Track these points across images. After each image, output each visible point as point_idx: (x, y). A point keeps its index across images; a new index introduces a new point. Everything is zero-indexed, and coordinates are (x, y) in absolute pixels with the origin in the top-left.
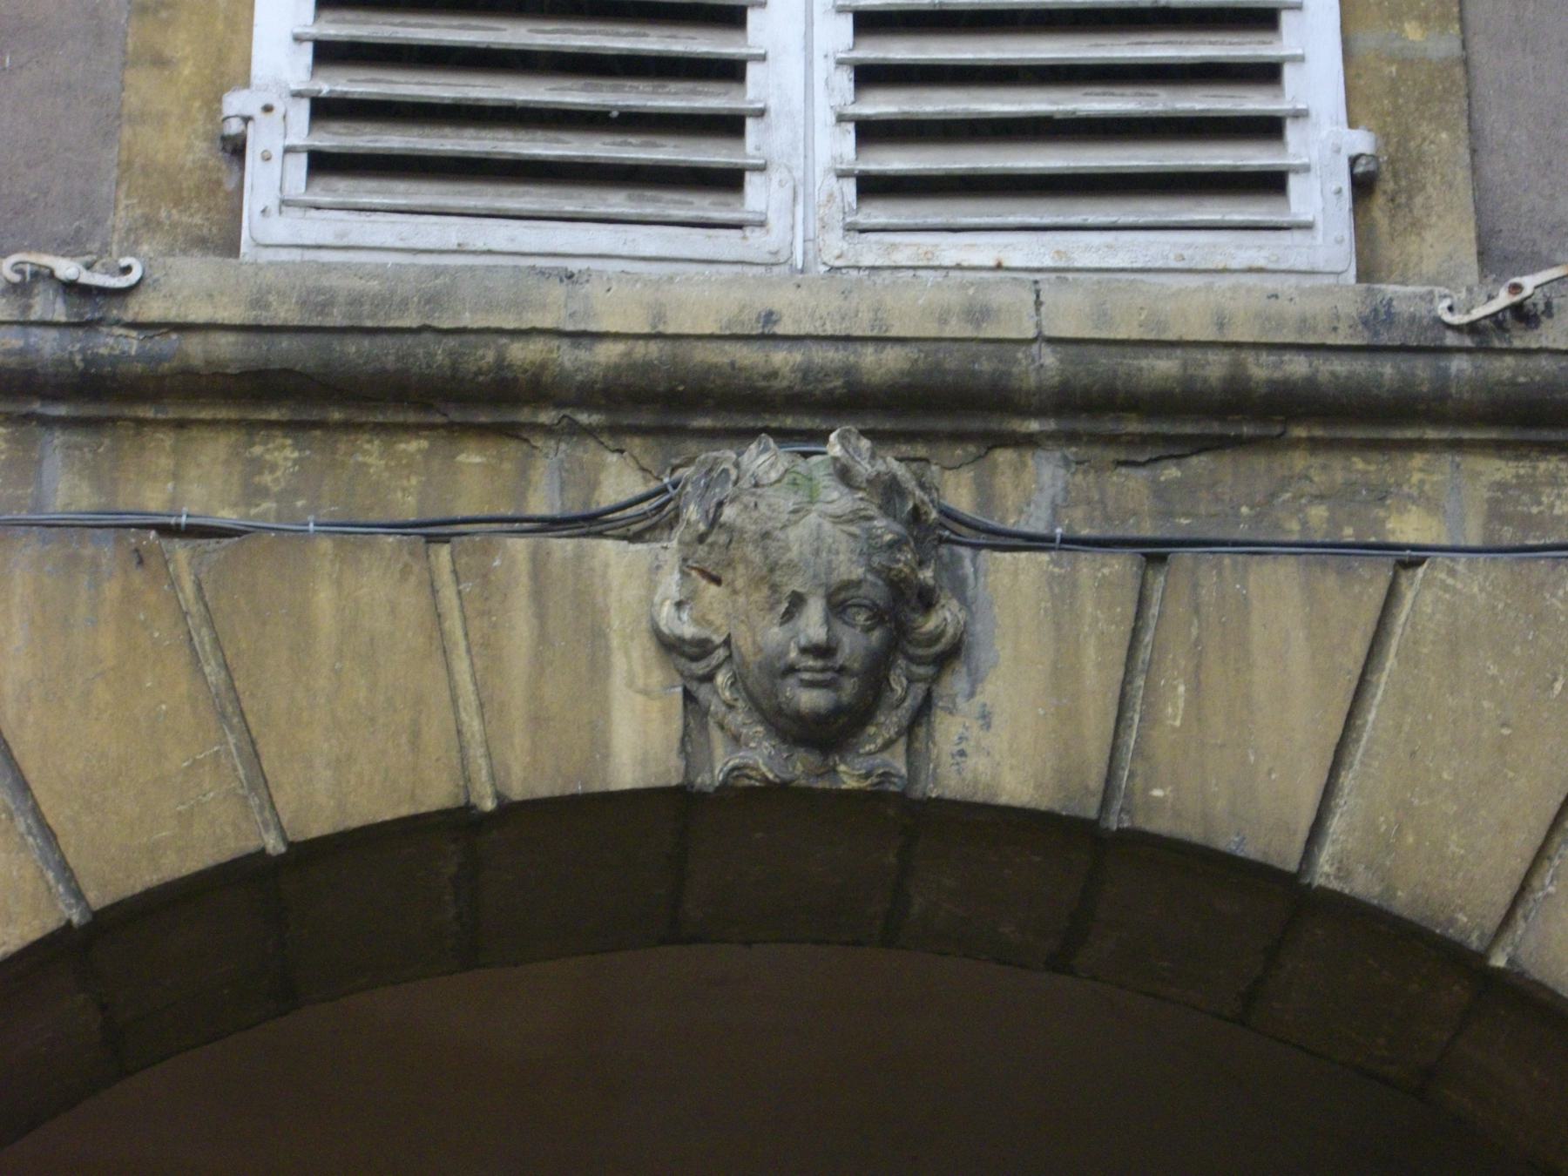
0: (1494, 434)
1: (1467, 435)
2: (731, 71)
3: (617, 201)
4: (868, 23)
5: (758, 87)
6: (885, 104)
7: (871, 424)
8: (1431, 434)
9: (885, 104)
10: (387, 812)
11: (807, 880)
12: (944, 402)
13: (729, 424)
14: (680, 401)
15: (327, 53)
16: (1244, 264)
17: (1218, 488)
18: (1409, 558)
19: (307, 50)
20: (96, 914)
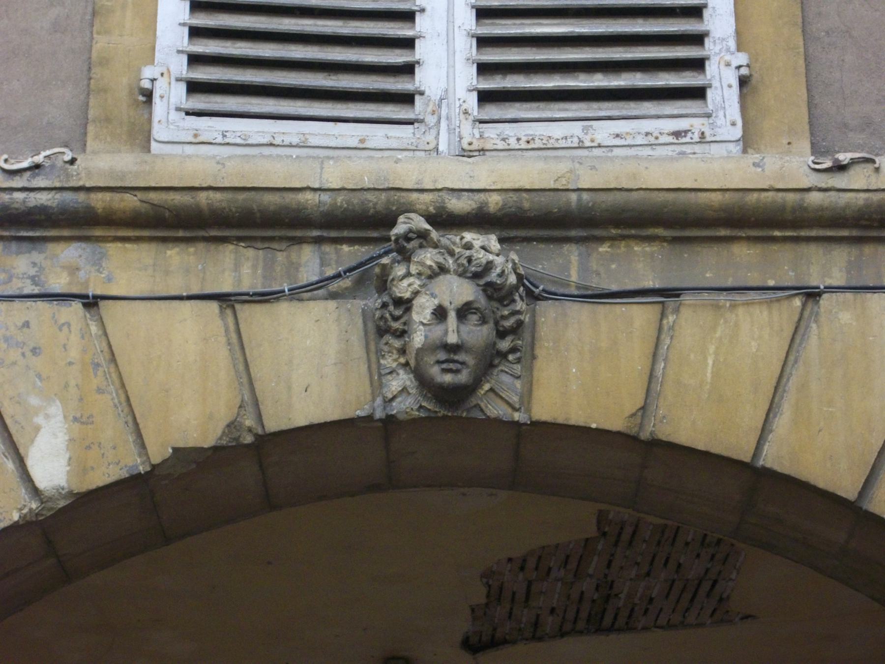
0: (855, 233)
1: (325, 234)
2: (408, 43)
3: (648, 107)
4: (483, 13)
5: (421, 51)
6: (205, 74)
7: (505, 234)
8: (777, 233)
9: (205, 74)
10: (701, 445)
11: (443, 443)
12: (529, 221)
13: (13, 233)
14: (364, 223)
15: (196, 32)
16: (633, 149)
17: (709, 264)
18: (812, 295)
19: (186, 30)
20: (154, 467)
